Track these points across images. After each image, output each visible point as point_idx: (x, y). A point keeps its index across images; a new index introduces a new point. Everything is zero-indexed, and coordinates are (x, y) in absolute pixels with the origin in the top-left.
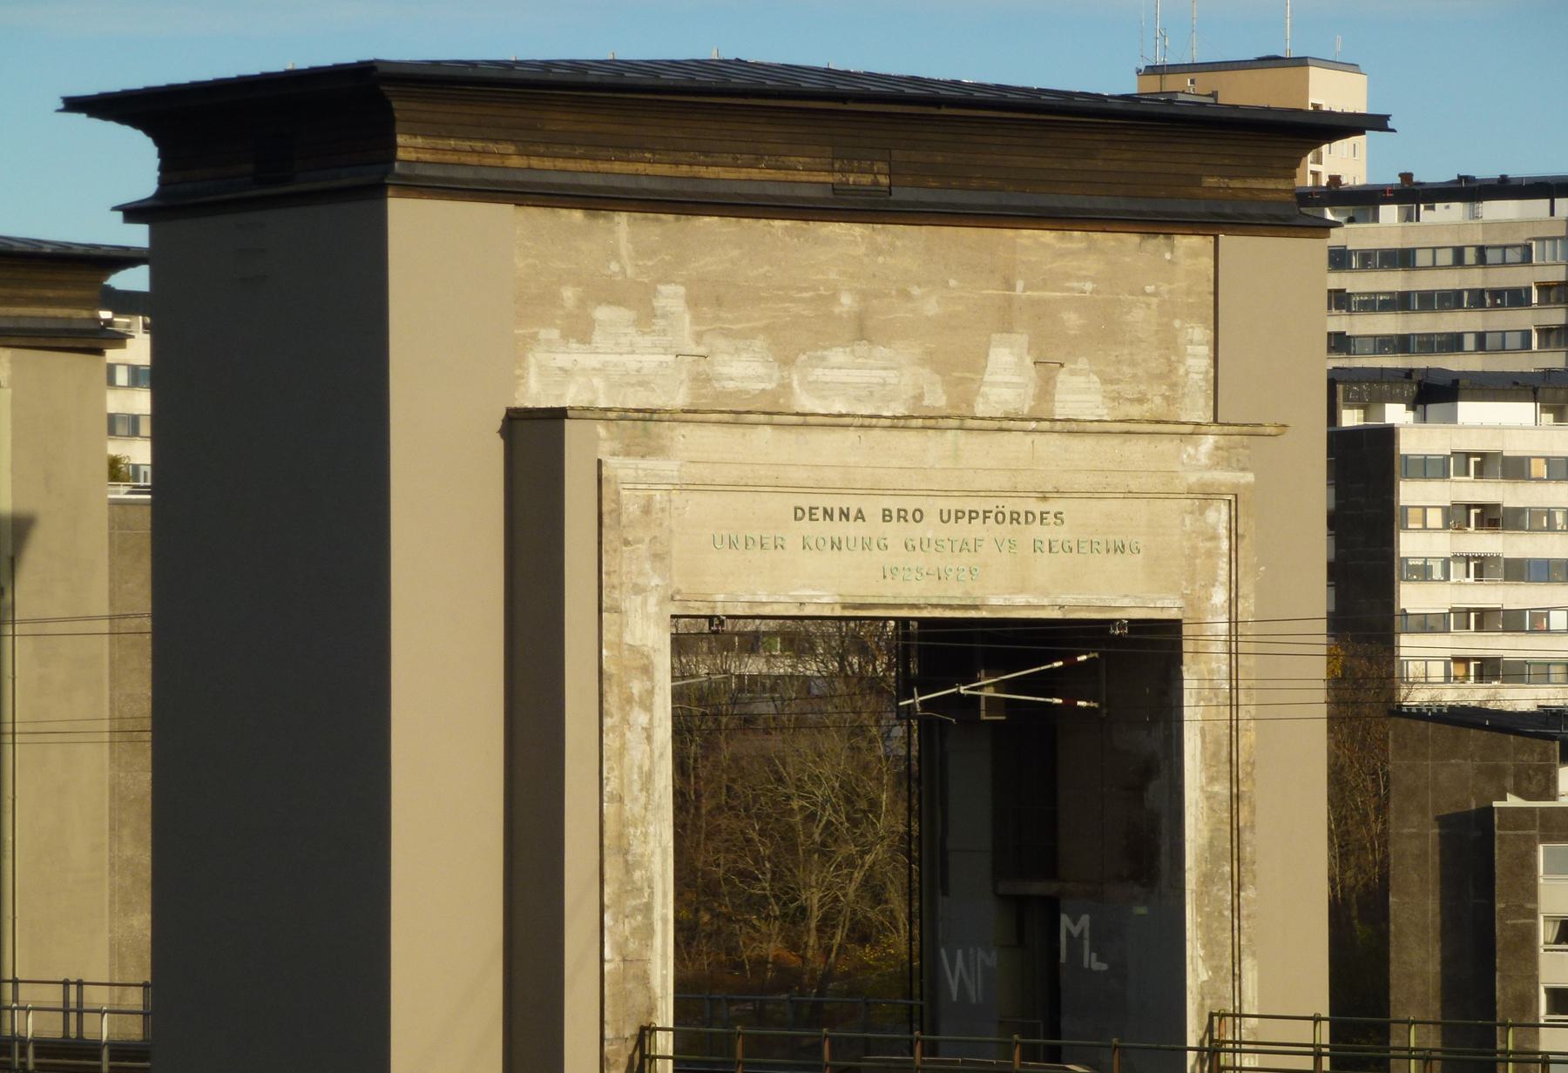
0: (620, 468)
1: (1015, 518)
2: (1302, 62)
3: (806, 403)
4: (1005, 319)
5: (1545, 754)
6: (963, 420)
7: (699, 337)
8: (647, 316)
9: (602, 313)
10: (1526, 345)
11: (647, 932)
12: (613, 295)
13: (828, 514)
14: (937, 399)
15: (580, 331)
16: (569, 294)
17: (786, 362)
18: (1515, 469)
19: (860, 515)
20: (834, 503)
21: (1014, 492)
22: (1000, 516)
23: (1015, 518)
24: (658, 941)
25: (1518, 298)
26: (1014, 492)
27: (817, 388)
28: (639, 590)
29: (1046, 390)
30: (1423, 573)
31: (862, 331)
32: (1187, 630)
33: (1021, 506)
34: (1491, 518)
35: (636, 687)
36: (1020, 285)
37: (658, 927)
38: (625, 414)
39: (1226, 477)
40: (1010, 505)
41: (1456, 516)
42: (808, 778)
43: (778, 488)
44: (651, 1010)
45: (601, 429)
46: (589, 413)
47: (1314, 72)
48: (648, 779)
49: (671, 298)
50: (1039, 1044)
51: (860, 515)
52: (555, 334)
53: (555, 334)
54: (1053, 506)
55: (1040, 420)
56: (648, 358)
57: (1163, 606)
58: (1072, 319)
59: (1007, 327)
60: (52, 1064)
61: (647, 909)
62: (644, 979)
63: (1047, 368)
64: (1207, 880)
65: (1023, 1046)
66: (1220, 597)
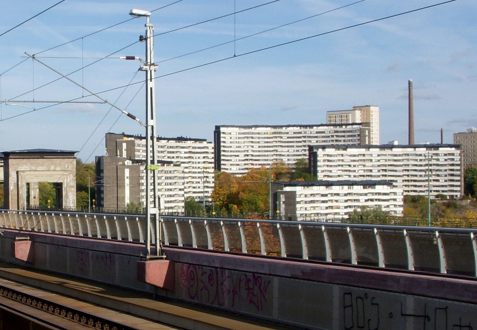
0: (21, 174)
2: (370, 106)
3: (38, 170)
4: (52, 164)
5: (282, 186)
6: (49, 171)
8: (27, 165)
10: (356, 141)
11: (24, 201)
15: (22, 166)
16: (21, 164)
18: (331, 156)
25: (355, 136)
27: (39, 169)
29: (55, 168)
30: (321, 166)
31: (42, 165)
32: (63, 183)
34: (329, 161)
41: (324, 161)
42: (221, 188)
43: (33, 175)
46: (20, 171)
47: (371, 107)
49: (28, 164)
56: (27, 167)
57: (61, 181)
62: (24, 204)
63: (56, 167)
64: (65, 197)
66: (66, 181)
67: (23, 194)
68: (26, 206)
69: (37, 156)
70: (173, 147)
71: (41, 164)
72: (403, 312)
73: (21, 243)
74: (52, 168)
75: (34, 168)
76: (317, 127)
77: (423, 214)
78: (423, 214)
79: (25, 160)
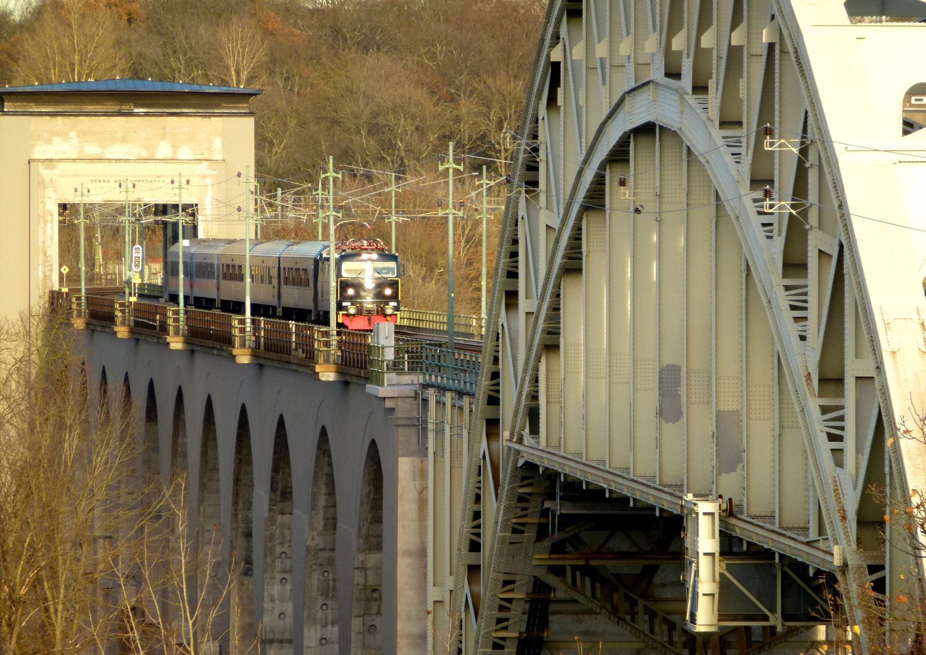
1: (151, 182)
7: (80, 143)
8: (66, 138)
9: (54, 138)
11: (51, 270)
12: (57, 134)
13: (100, 181)
14: (145, 155)
15: (49, 142)
16: (46, 135)
17: (103, 147)
19: (108, 181)
20: (102, 179)
21: (149, 176)
22: (147, 181)
23: (151, 182)
24: (54, 272)
26: (149, 176)
28: (50, 198)
29: (175, 152)
31: (124, 140)
33: (152, 179)
35: (49, 218)
36: (168, 129)
37: (54, 269)
38: (45, 160)
39: (209, 172)
40: (149, 179)
44: (53, 286)
45: (40, 164)
48: (52, 238)
49: (73, 134)
50: (80, 285)
51: (108, 181)
52: (42, 143)
53: (42, 143)
54: (161, 179)
55: (173, 160)
58: (182, 137)
59: (164, 138)
60: (461, 452)
61: (52, 265)
63: (175, 147)
65: (265, 321)
67: (48, 243)
68: (40, 284)
69: (161, 106)
70: (802, 67)
71: (120, 134)
72: (363, 574)
73: (741, 283)
74: (165, 149)
75: (92, 150)
76: (547, 6)
77: (65, 290)
78: (65, 290)
79: (60, 120)
